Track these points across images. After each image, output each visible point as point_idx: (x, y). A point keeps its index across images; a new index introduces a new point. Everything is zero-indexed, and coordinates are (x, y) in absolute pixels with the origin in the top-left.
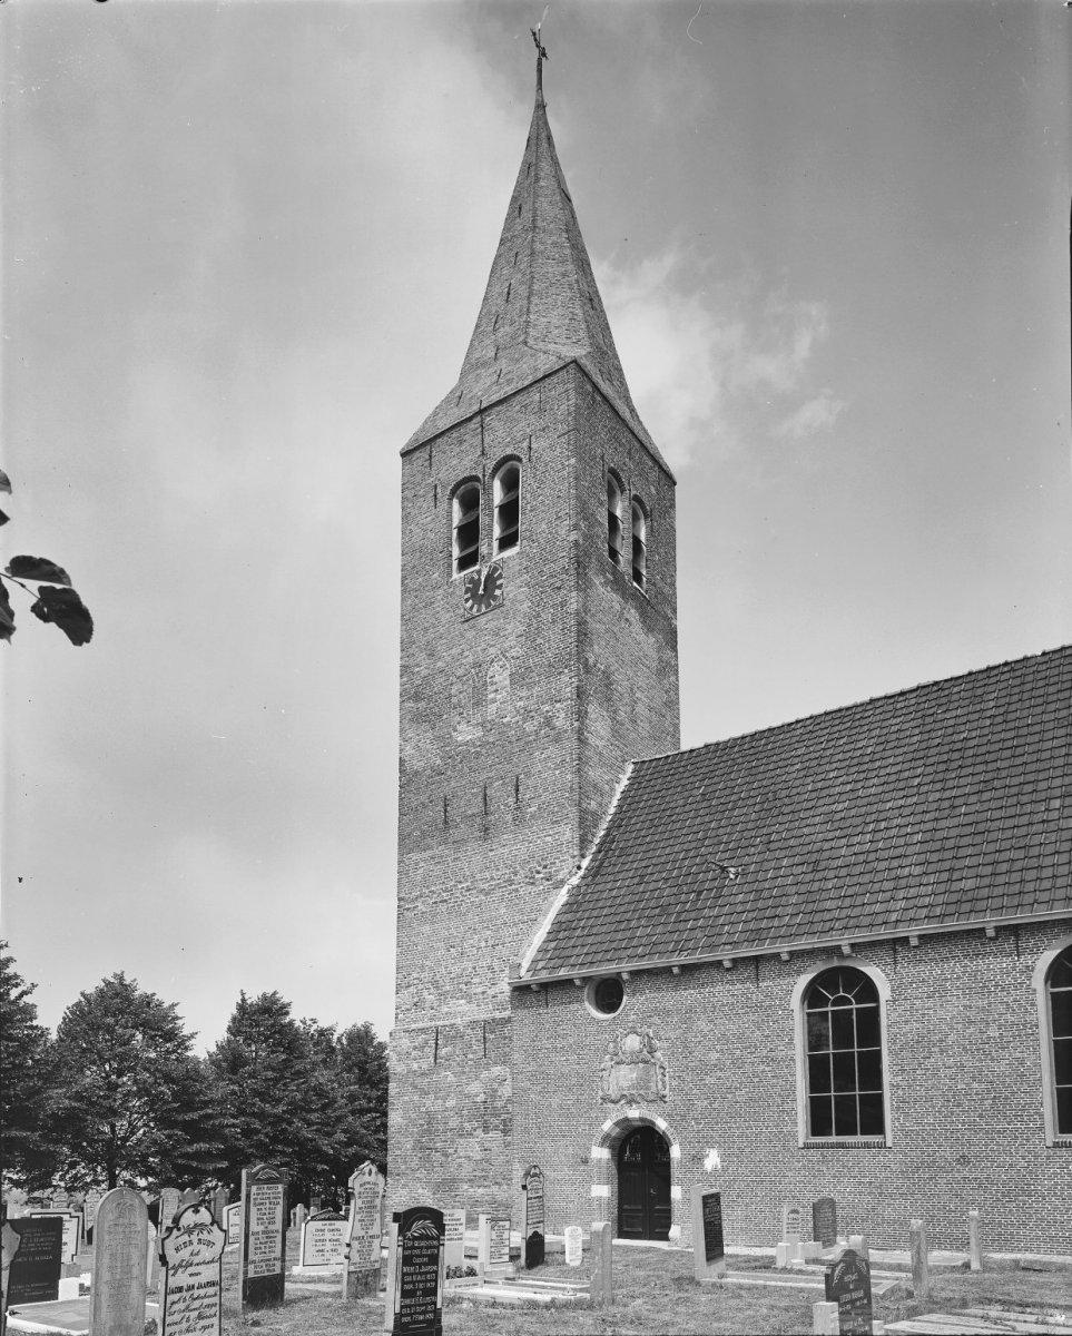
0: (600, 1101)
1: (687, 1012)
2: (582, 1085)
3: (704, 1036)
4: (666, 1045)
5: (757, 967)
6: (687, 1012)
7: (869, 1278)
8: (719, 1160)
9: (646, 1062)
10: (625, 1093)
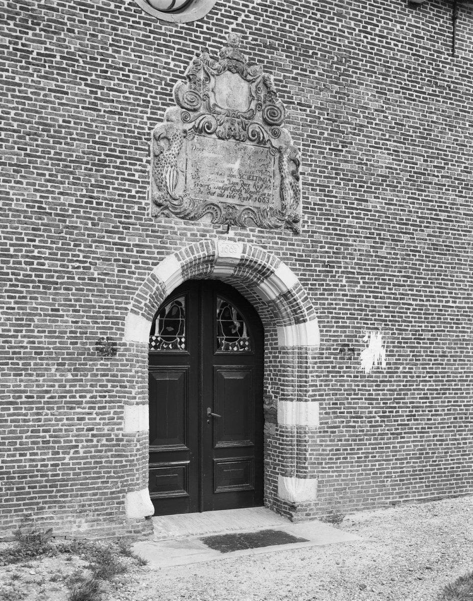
0: (152, 209)
1: (339, 62)
2: (102, 164)
3: (370, 120)
5: (454, 19)
6: (339, 62)
8: (383, 352)
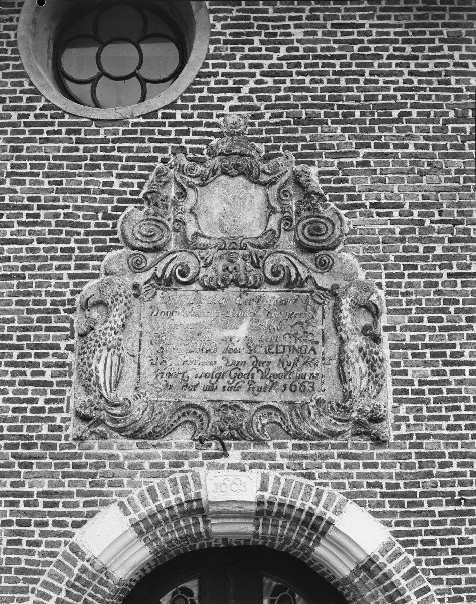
0: (74, 428)
4: (376, 225)
7: (153, 571)
9: (293, 284)
10: (196, 397)
